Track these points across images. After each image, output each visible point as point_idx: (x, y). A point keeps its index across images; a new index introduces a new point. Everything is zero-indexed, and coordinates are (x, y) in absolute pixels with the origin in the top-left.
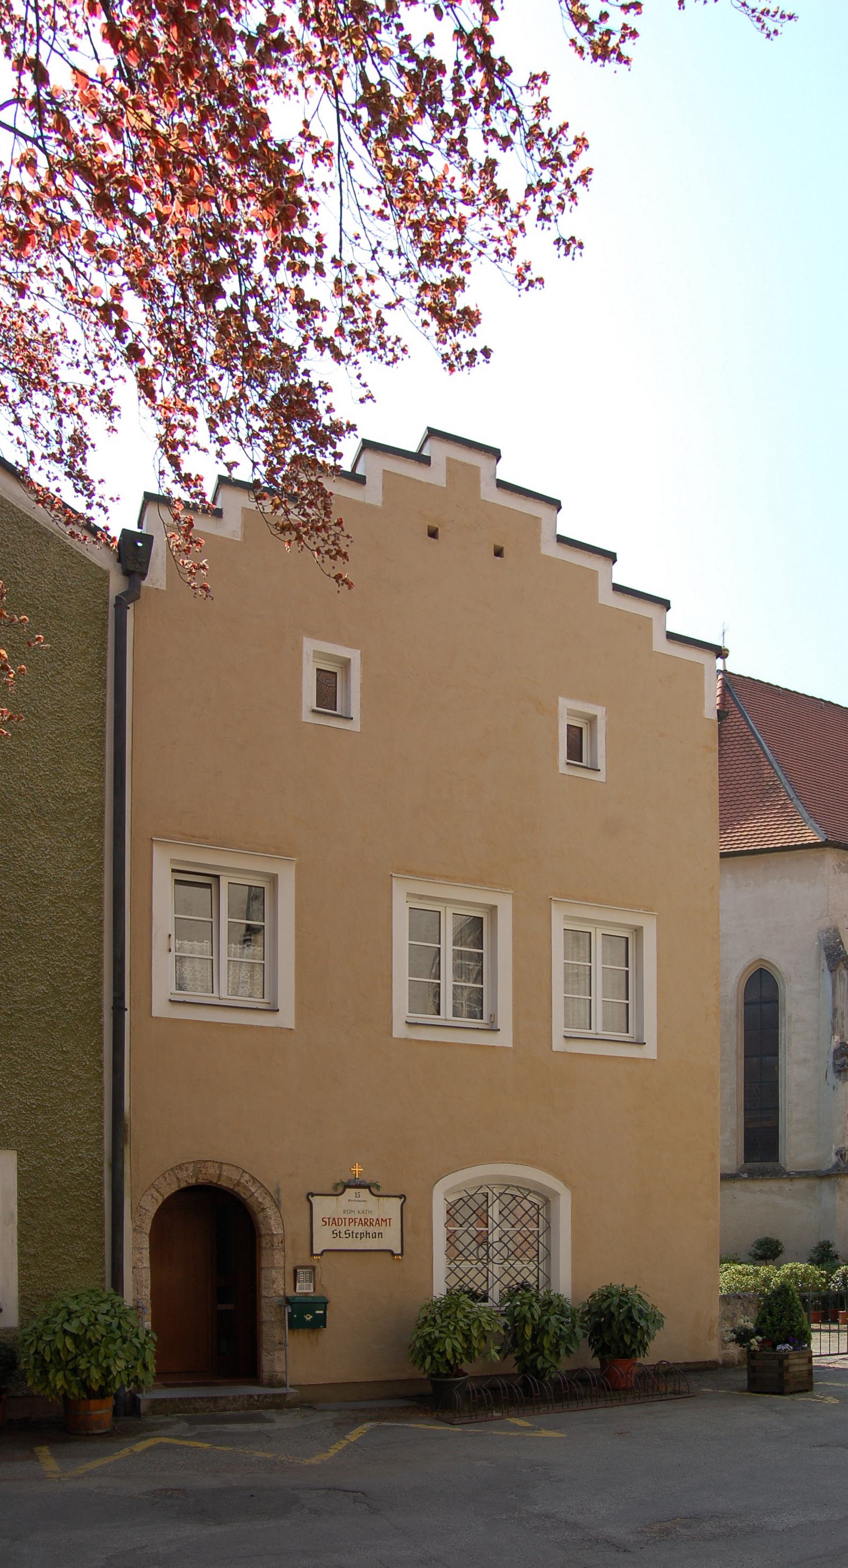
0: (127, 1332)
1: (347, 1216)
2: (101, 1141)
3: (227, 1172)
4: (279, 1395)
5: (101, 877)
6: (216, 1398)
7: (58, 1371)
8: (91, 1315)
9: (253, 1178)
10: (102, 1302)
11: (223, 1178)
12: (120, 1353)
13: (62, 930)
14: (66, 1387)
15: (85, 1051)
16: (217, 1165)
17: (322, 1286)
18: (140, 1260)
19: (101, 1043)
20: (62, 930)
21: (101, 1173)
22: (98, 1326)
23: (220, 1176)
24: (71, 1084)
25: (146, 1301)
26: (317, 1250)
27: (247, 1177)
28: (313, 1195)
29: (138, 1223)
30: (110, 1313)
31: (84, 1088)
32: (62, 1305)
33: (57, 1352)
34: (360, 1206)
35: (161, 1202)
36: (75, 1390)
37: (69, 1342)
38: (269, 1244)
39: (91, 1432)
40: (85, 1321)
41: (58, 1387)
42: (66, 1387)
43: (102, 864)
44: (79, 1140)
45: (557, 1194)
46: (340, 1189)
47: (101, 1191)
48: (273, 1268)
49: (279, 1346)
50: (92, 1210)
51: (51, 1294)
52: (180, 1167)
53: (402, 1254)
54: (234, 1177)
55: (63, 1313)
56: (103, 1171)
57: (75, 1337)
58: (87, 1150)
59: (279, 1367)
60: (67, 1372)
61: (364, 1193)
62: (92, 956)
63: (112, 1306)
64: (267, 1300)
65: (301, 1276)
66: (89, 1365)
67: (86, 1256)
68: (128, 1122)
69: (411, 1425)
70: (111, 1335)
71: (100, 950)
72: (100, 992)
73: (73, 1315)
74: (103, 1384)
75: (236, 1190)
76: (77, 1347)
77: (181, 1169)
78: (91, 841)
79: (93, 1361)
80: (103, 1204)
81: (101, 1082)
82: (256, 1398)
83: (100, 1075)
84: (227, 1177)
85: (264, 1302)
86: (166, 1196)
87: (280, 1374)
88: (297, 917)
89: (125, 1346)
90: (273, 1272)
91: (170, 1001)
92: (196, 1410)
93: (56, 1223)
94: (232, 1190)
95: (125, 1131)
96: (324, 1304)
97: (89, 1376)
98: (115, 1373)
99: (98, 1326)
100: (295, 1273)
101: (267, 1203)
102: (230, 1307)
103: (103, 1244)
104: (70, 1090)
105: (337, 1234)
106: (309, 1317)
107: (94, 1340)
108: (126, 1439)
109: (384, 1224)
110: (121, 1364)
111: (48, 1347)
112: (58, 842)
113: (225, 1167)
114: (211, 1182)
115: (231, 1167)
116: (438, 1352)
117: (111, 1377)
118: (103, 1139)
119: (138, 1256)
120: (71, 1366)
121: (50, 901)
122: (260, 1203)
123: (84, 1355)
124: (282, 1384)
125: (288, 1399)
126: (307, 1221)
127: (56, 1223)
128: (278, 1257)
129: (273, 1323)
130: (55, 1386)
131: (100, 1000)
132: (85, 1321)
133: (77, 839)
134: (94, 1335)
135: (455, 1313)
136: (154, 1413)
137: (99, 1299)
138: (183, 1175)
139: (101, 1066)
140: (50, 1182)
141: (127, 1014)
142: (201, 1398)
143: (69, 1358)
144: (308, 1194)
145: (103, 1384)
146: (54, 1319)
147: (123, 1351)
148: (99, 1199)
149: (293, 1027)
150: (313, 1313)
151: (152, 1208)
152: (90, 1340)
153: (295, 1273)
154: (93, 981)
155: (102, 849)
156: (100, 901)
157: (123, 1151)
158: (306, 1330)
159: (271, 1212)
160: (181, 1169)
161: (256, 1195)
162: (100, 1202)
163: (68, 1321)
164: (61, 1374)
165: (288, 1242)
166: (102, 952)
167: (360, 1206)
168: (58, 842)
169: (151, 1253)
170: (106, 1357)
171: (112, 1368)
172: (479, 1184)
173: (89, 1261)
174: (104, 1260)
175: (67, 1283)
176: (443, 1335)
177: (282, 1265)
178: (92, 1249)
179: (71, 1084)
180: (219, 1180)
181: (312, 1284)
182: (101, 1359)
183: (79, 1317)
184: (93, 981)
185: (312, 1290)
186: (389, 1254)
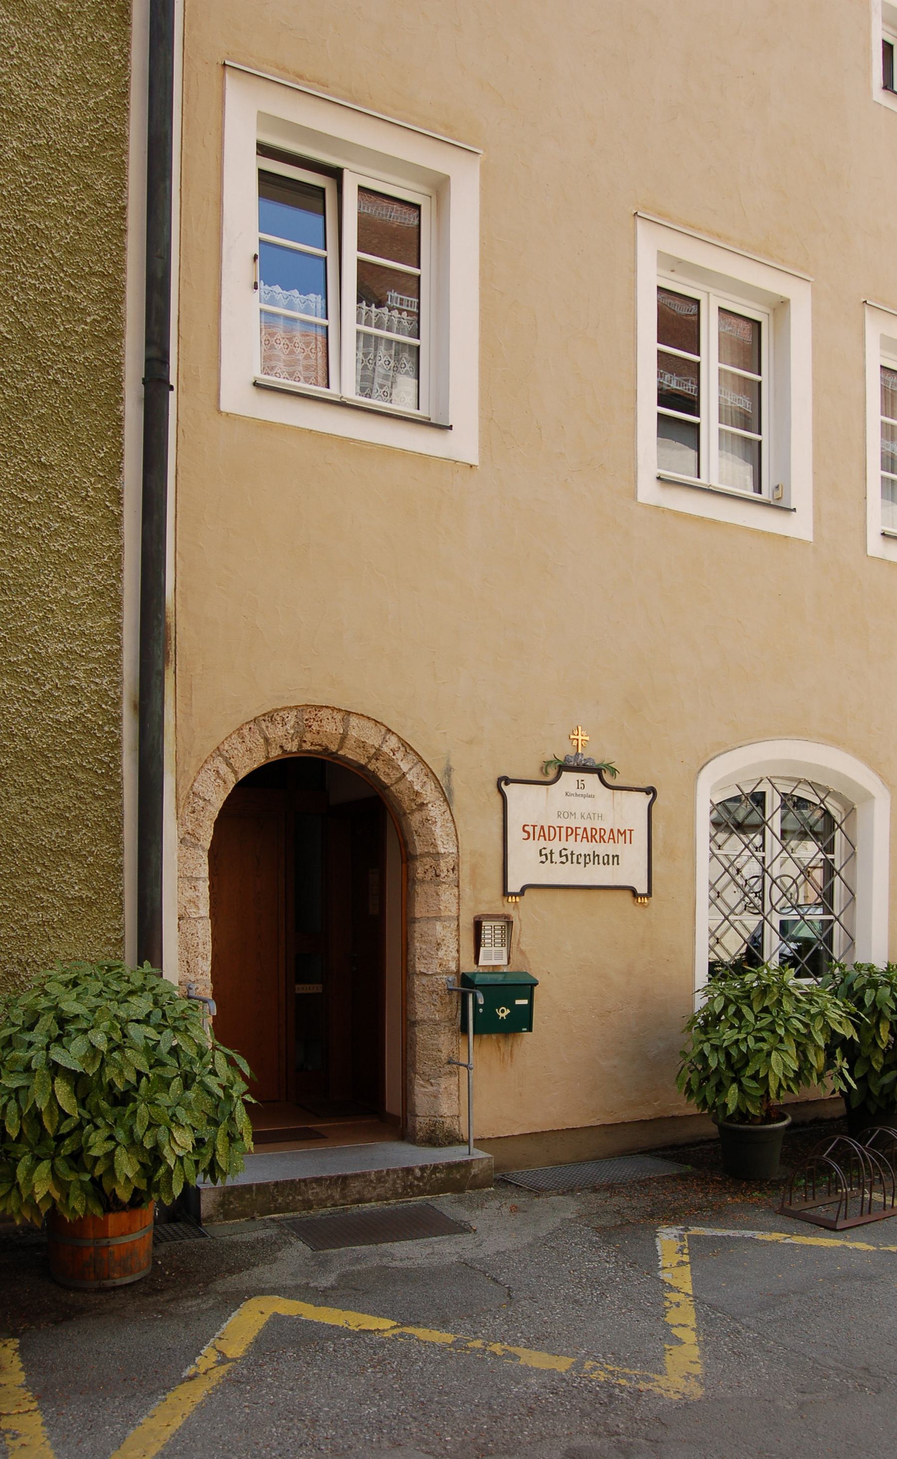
0: (191, 1062)
1: (565, 823)
2: (116, 655)
3: (358, 730)
4: (458, 1166)
5: (124, 122)
6: (345, 1178)
7: (38, 1160)
8: (113, 1027)
9: (404, 744)
10: (131, 993)
11: (350, 743)
12: (181, 1112)
13: (42, 215)
14: (57, 1195)
15: (85, 469)
16: (338, 717)
17: (522, 952)
18: (193, 902)
19: (118, 454)
20: (42, 215)
21: (117, 721)
22: (129, 1053)
23: (344, 737)
24: (57, 533)
25: (204, 987)
26: (514, 887)
27: (393, 742)
28: (508, 781)
29: (190, 827)
30: (154, 1019)
31: (83, 543)
32: (44, 1003)
33: (36, 1116)
34: (581, 805)
35: (231, 786)
36: (78, 1204)
37: (62, 1090)
38: (431, 874)
39: (109, 1283)
40: (99, 1040)
41: (38, 1198)
42: (57, 1195)
43: (125, 95)
44: (71, 652)
45: (869, 797)
46: (552, 772)
47: (116, 760)
48: (438, 918)
49: (448, 1068)
50: (98, 798)
51: (13, 975)
52: (270, 716)
53: (649, 894)
54: (370, 742)
55: (47, 1022)
56: (120, 718)
57: (76, 1079)
58: (91, 672)
59: (446, 1108)
60: (58, 1162)
61: (592, 780)
62: (103, 275)
63: (156, 1003)
64: (425, 980)
65: (486, 933)
66: (110, 1145)
67: (85, 893)
68: (170, 620)
69: (759, 1235)
70: (159, 1070)
71: (120, 266)
72: (118, 351)
73: (71, 1028)
74: (143, 1186)
75: (371, 767)
76: (82, 1103)
77: (272, 720)
78: (105, 46)
79: (120, 1135)
80: (120, 786)
81: (119, 535)
82: (418, 1173)
83: (117, 520)
84: (357, 740)
85: (418, 984)
86: (242, 774)
87: (448, 1121)
88: (483, 260)
89: (191, 1095)
90: (439, 926)
91: (255, 384)
92: (308, 1205)
93: (24, 824)
94: (363, 767)
95: (167, 639)
96: (528, 988)
97: (111, 1170)
98: (171, 1161)
99: (129, 1053)
100: (478, 927)
101: (429, 793)
102: (315, 988)
103: (120, 870)
104: (55, 546)
105: (546, 857)
106: (503, 1013)
107: (120, 1086)
108: (192, 1304)
109: (621, 838)
110: (185, 1139)
111: (12, 1105)
112: (37, 36)
113: (354, 720)
114: (326, 749)
115: (365, 722)
116: (755, 1077)
117: (162, 1170)
118: (120, 651)
119: (190, 893)
120: (68, 1147)
121: (20, 153)
122: (417, 794)
123: (99, 1121)
124: (453, 1139)
125: (474, 1171)
126: (499, 831)
127: (24, 824)
128: (447, 896)
129: (437, 1023)
130: (32, 1195)
131: (118, 366)
132: (99, 1040)
133: (77, 37)
134: (121, 1072)
135: (779, 1002)
136: (227, 1216)
137: (125, 987)
138: (277, 732)
139: (119, 502)
140: (12, 736)
141: (172, 395)
142: (318, 1181)
143: (64, 1130)
144: (500, 780)
145: (143, 1186)
146: (28, 1037)
147: (188, 1107)
148: (112, 774)
149: (475, 462)
150: (511, 1005)
151: (217, 798)
152: (111, 1085)
153: (478, 927)
154: (105, 326)
155: (125, 67)
156: (121, 169)
157: (161, 674)
158: (494, 1037)
159: (436, 810)
160: (272, 720)
161: (409, 777)
162: (113, 783)
163: (58, 1039)
164: (44, 1168)
165: (465, 870)
166: (123, 271)
167: (581, 805)
168: (37, 36)
169: (211, 888)
170: (152, 1125)
171: (166, 1152)
172: (758, 776)
173: (91, 904)
174: (122, 903)
175: (46, 949)
176: (765, 1047)
177: (454, 913)
178: (98, 879)
179: (57, 533)
180: (341, 747)
181: (504, 949)
182: (139, 1130)
183: (85, 1031)
184: (105, 326)
185: (504, 961)
186: (628, 895)
